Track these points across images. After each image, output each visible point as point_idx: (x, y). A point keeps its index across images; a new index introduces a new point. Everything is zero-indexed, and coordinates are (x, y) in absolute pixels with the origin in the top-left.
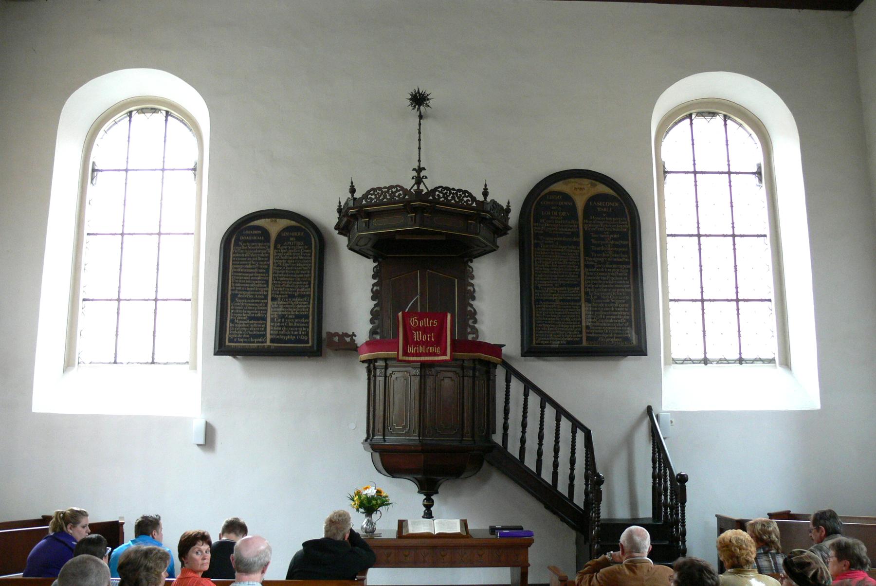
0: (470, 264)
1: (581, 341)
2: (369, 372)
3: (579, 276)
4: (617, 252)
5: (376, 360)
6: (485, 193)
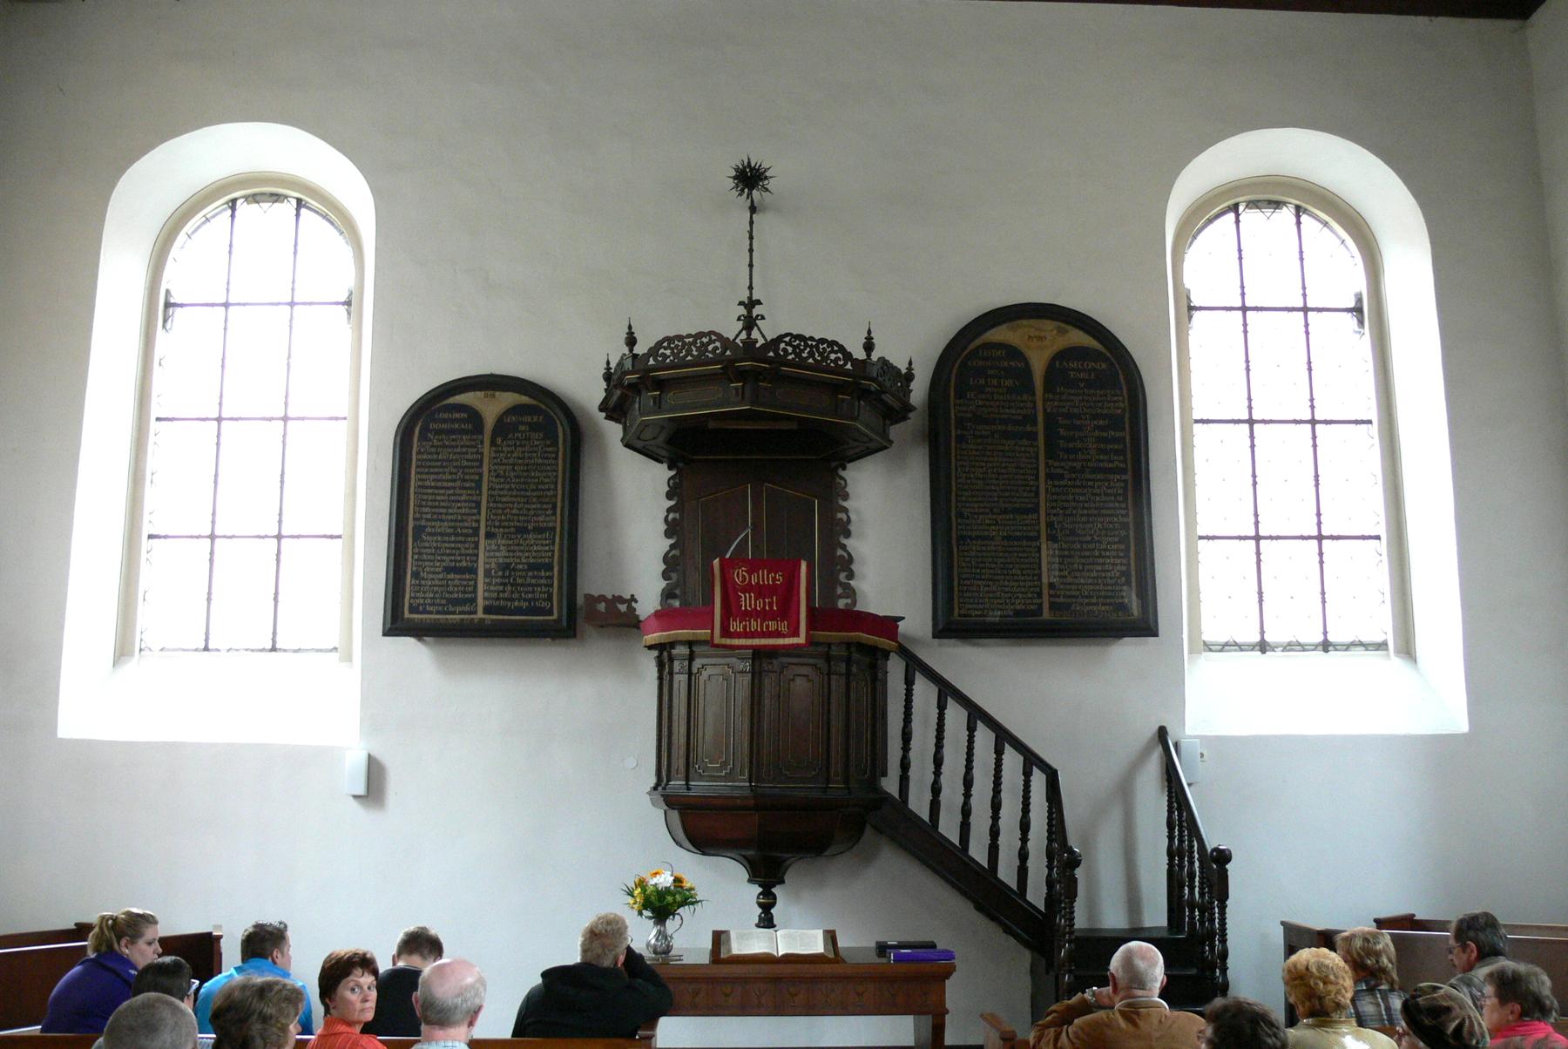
0: (842, 473)
1: (1039, 611)
2: (660, 665)
3: (1037, 494)
4: (1105, 452)
5: (672, 645)
6: (869, 346)
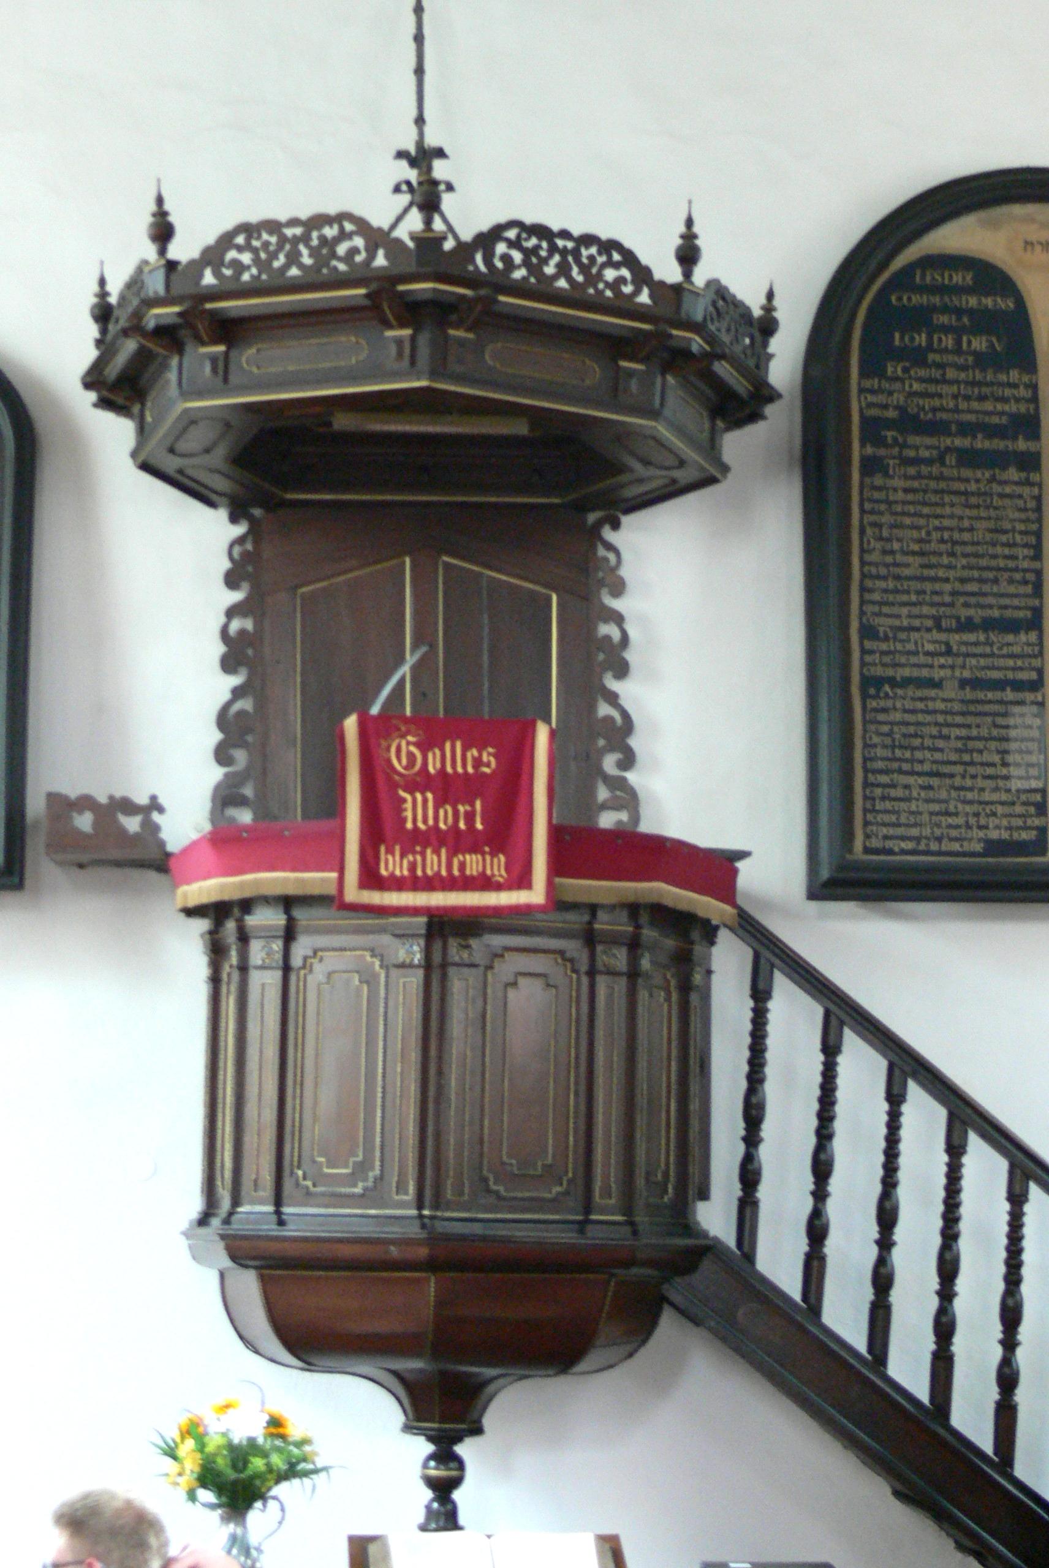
0: (608, 534)
2: (216, 951)
5: (247, 905)
6: (688, 255)
